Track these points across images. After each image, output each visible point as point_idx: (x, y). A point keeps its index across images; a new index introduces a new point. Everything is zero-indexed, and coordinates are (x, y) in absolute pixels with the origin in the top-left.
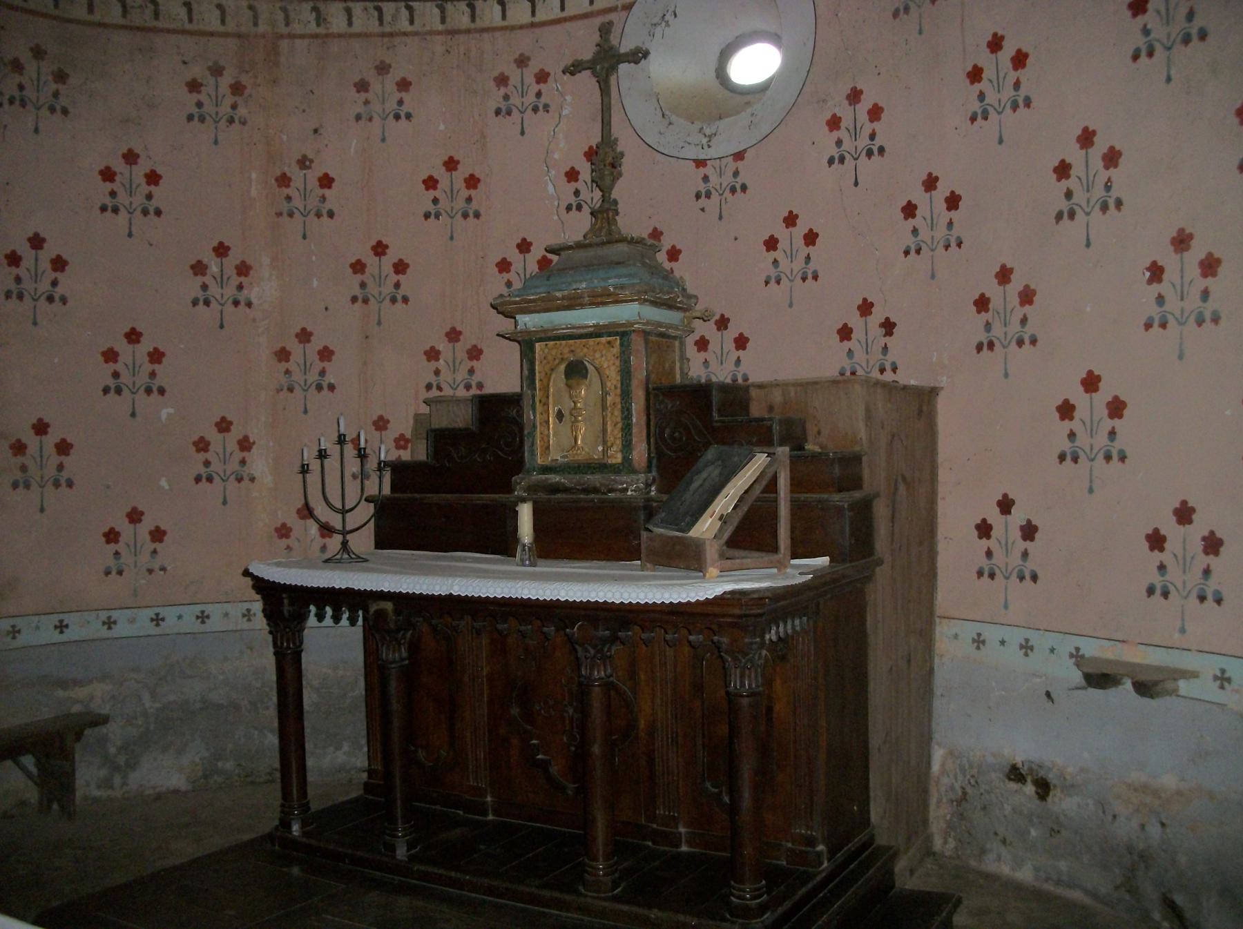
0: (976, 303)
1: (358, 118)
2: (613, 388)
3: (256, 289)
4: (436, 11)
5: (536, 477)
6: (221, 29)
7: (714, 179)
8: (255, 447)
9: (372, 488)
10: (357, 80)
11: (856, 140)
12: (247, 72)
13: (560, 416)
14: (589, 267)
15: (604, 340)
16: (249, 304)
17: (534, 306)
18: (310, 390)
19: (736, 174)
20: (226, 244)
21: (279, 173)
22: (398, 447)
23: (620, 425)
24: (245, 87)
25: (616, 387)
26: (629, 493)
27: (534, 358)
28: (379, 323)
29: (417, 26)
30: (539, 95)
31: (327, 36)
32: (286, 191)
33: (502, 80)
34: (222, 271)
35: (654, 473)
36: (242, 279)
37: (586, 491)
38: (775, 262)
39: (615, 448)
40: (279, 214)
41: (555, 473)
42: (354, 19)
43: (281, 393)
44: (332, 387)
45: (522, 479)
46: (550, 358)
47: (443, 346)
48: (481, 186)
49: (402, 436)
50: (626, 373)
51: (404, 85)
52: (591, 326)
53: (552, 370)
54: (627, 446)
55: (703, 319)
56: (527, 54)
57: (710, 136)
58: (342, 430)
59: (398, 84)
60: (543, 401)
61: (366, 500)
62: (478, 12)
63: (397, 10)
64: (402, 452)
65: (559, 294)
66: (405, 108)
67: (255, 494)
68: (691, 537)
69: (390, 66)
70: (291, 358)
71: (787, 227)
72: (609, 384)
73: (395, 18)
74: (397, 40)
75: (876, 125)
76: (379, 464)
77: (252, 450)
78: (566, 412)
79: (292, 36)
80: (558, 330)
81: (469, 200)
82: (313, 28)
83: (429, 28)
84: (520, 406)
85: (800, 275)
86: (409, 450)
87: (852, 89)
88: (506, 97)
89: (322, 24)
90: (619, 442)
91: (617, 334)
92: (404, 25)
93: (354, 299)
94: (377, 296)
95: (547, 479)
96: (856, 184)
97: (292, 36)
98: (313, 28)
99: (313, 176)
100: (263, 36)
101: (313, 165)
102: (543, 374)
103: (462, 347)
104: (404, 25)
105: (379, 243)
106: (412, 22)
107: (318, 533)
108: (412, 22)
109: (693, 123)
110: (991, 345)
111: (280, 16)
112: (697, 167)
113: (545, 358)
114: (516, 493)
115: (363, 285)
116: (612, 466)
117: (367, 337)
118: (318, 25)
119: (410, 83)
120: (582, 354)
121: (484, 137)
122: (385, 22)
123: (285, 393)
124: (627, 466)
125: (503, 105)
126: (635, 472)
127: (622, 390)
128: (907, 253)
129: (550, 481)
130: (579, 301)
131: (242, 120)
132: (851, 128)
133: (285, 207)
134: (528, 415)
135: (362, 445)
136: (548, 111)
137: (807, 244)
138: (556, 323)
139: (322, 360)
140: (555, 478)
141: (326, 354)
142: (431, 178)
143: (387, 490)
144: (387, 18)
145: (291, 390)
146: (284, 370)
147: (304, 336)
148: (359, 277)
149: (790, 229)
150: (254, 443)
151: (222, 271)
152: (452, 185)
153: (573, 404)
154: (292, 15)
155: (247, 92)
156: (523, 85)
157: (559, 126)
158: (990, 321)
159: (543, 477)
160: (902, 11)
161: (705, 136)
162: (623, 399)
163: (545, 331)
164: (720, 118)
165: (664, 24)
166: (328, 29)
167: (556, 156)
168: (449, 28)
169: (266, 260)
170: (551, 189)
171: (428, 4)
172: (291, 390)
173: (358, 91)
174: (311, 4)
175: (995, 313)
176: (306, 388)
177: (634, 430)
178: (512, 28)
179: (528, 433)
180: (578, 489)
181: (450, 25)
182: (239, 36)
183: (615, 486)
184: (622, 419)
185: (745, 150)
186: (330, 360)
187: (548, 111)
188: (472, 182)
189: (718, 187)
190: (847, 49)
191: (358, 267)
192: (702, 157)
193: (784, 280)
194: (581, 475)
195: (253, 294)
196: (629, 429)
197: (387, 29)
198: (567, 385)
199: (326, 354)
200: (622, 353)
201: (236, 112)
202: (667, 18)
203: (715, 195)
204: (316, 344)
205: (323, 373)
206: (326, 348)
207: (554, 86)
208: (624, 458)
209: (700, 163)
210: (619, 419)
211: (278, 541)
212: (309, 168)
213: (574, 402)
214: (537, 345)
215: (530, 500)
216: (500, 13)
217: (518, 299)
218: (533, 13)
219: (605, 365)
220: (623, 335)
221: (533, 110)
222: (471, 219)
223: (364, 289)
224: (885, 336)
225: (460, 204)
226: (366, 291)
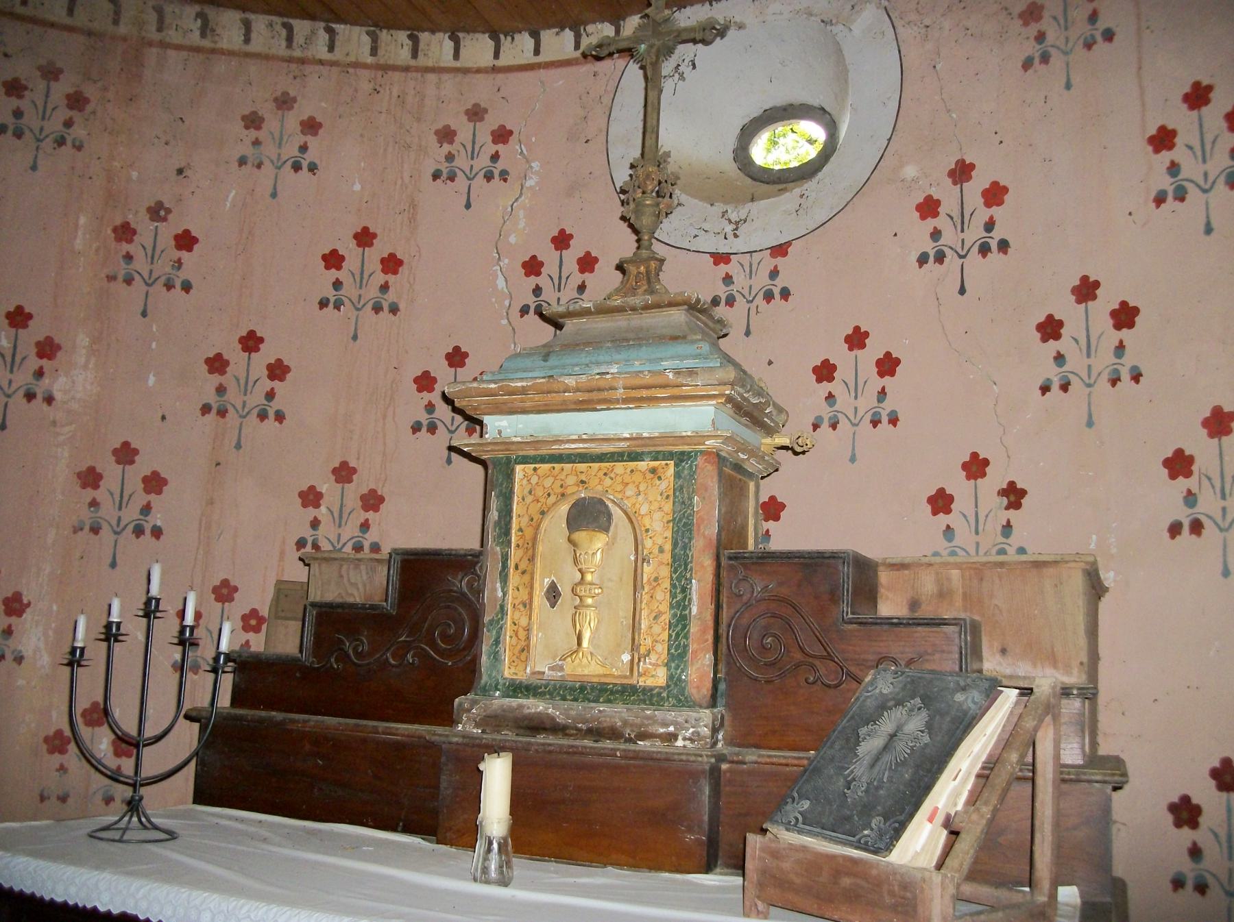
0: (932, 500)
1: (242, 162)
2: (656, 551)
3: (62, 380)
4: (366, 39)
5: (499, 702)
6: (67, 21)
7: (740, 281)
8: (28, 610)
9: (199, 695)
10: (247, 113)
11: (962, 231)
12: (95, 82)
13: (553, 594)
14: (621, 341)
15: (643, 465)
16: (49, 400)
17: (522, 401)
18: (124, 533)
19: (774, 274)
20: (27, 310)
21: (118, 222)
22: (247, 628)
23: (666, 617)
24: (87, 101)
25: (661, 550)
26: (680, 743)
27: (512, 492)
28: (238, 446)
29: (338, 55)
30: (495, 157)
31: (213, 51)
32: (125, 247)
33: (446, 135)
34: (15, 347)
35: (720, 709)
36: (44, 362)
37: (596, 733)
38: (830, 397)
39: (653, 658)
40: (111, 278)
41: (535, 695)
42: (254, 35)
43: (80, 533)
44: (157, 533)
45: (474, 703)
46: (539, 492)
47: (327, 486)
48: (403, 270)
49: (254, 613)
50: (683, 527)
51: (311, 126)
52: (626, 439)
53: (543, 513)
54: (678, 655)
55: (792, 449)
56: (483, 105)
57: (737, 223)
58: (155, 590)
59: (302, 123)
60: (522, 566)
61: (187, 717)
62: (422, 46)
63: (313, 32)
64: (251, 636)
65: (571, 381)
66: (310, 156)
67: (21, 682)
68: (894, 871)
69: (294, 100)
70: (101, 483)
71: (851, 349)
72: (648, 543)
73: (309, 40)
74: (308, 69)
75: (995, 211)
76: (216, 659)
77: (24, 615)
78: (565, 589)
79: (164, 45)
80: (562, 442)
81: (385, 288)
82: (195, 38)
83: (353, 59)
84: (475, 573)
85: (868, 417)
86: (263, 635)
87: (957, 162)
88: (450, 157)
89: (209, 37)
90: (662, 648)
91: (669, 456)
92: (321, 51)
93: (206, 409)
94: (239, 407)
95: (521, 706)
96: (962, 291)
97: (164, 45)
98: (195, 38)
99: (167, 232)
100: (125, 39)
101: (170, 217)
102: (525, 520)
103: (354, 491)
104: (321, 51)
105: (252, 334)
106: (331, 48)
107: (111, 749)
108: (331, 48)
109: (712, 205)
110: (1197, 527)
111: (152, 17)
112: (716, 263)
113: (530, 493)
114: (460, 727)
115: (221, 390)
116: (647, 691)
117: (218, 464)
118: (203, 35)
119: (320, 125)
120: (600, 488)
121: (413, 205)
122: (295, 44)
123: (85, 534)
124: (675, 694)
125: (444, 168)
126: (693, 705)
127: (673, 556)
128: (1045, 389)
129: (526, 711)
130: (605, 395)
131: (77, 144)
132: (956, 214)
133: (122, 269)
134: (493, 590)
135: (189, 619)
136: (505, 180)
137: (881, 374)
138: (556, 432)
139: (148, 491)
140: (536, 706)
141: (155, 483)
142: (334, 252)
143: (224, 700)
144: (299, 39)
145: (95, 530)
146: (89, 500)
147: (126, 454)
148: (216, 379)
149: (856, 352)
150: (29, 604)
151: (15, 347)
152: (363, 266)
153: (579, 575)
154: (168, 20)
155: (89, 108)
156: (474, 143)
157: (520, 200)
158: (1195, 490)
159: (514, 702)
160: (1037, 61)
161: (730, 222)
162: (675, 572)
163: (536, 443)
164: (752, 200)
165: (677, 76)
166: (215, 42)
167: (512, 239)
168: (382, 61)
169: (83, 340)
170: (501, 283)
171: (357, 29)
172: (95, 530)
173: (247, 127)
174: (197, 8)
175: (1203, 478)
176: (119, 530)
177: (694, 629)
178: (466, 71)
179: (491, 622)
180: (579, 730)
181: (382, 59)
182: (90, 33)
183: (652, 729)
184: (672, 607)
185: (789, 244)
186: (159, 492)
187: (505, 180)
188: (392, 264)
189: (746, 292)
190: (949, 111)
191: (217, 364)
192: (723, 249)
193: (843, 425)
194: (586, 704)
195: (58, 385)
196: (684, 627)
197: (297, 53)
198: (570, 540)
199: (155, 483)
200: (678, 489)
201: (71, 131)
202: (681, 69)
203: (740, 301)
204: (143, 466)
205: (146, 510)
206: (155, 474)
207: (518, 147)
208: (670, 677)
209: (720, 258)
210: (665, 607)
211: (47, 757)
212: (164, 219)
213: (580, 570)
214: (518, 468)
215: (510, 749)
216: (452, 52)
217: (493, 386)
218: (497, 55)
219: (644, 510)
220: (681, 458)
221: (485, 176)
222: (385, 314)
223: (222, 396)
224: (1007, 508)
225: (372, 292)
226: (225, 398)
